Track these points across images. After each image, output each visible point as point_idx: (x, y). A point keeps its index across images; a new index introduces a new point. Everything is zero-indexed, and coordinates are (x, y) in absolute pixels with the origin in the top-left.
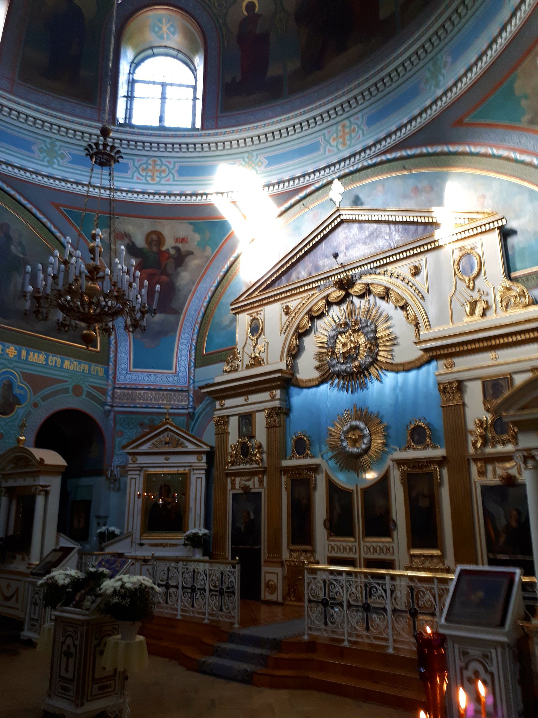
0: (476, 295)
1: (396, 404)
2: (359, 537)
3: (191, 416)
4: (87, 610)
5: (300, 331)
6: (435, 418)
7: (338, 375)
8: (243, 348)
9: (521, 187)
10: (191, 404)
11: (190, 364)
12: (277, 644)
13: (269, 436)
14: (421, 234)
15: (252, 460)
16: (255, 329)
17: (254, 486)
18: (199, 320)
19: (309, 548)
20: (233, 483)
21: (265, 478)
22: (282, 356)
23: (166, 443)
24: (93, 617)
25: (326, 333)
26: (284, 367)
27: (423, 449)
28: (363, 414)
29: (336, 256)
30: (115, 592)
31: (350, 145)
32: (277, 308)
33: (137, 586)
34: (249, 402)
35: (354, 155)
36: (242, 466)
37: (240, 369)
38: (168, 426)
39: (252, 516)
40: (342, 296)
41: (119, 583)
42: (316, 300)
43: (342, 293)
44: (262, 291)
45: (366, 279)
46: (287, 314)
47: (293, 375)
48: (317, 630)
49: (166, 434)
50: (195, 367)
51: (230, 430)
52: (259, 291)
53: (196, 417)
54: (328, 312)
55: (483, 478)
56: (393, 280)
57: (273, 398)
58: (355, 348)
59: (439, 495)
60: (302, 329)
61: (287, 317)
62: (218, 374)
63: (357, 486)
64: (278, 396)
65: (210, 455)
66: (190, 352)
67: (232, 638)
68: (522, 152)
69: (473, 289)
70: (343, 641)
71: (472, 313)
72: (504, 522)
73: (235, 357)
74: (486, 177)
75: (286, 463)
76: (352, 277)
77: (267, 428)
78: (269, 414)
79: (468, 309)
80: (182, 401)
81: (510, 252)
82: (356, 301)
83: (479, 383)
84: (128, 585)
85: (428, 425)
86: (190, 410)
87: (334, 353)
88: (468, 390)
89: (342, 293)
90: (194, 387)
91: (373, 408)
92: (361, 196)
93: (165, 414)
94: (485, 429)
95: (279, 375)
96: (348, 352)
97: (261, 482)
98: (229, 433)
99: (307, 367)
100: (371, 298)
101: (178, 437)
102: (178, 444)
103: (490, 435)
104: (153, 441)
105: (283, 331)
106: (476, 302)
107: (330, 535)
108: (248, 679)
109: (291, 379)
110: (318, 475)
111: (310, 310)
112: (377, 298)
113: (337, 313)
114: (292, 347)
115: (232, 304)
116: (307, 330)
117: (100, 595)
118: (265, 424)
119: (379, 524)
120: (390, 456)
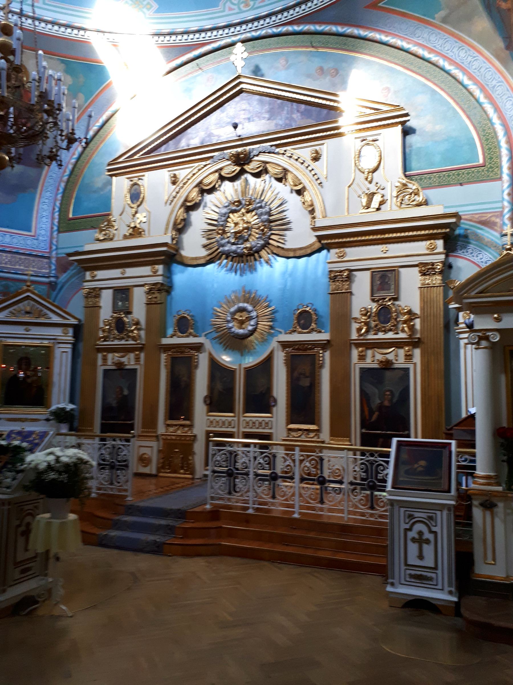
0: (373, 188)
1: (284, 290)
2: (239, 412)
3: (52, 286)
4: (8, 488)
5: (188, 204)
6: (321, 304)
7: (228, 255)
8: (121, 215)
9: (425, 85)
10: (53, 272)
11: (52, 228)
12: (181, 514)
13: (148, 313)
14: (317, 120)
15: (129, 337)
16: (136, 196)
17: (129, 362)
18: (65, 178)
19: (187, 422)
20: (105, 359)
21: (142, 355)
22: (167, 229)
23: (28, 313)
24: (17, 495)
25: (217, 210)
26: (169, 241)
27: (309, 333)
28: (251, 297)
29: (235, 126)
30: (50, 468)
31: (254, 5)
32: (165, 174)
33: (74, 460)
34: (126, 275)
35: (257, 19)
36: (116, 342)
37: (115, 239)
38: (29, 294)
39: (126, 392)
40: (236, 172)
41: (51, 458)
42: (207, 173)
43: (238, 168)
44: (142, 155)
45: (263, 158)
46: (174, 183)
47: (177, 250)
48: (220, 499)
49: (26, 302)
50: (59, 232)
51: (102, 304)
52: (141, 153)
53: (59, 287)
54: (220, 186)
55: (358, 362)
56: (292, 161)
57: (155, 273)
58: (247, 228)
59: (320, 375)
60: (190, 202)
61: (175, 186)
62: (88, 242)
63: (240, 365)
64: (160, 272)
65: (78, 329)
66: (53, 213)
67: (131, 510)
68: (431, 51)
69: (370, 182)
70: (247, 508)
71: (368, 207)
72: (378, 401)
73: (110, 225)
74: (391, 69)
75: (165, 341)
76: (250, 153)
77: (147, 304)
78: (150, 290)
79: (364, 201)
80: (41, 268)
81: (407, 150)
82: (251, 179)
83: (368, 274)
84: (64, 459)
85: (315, 310)
86: (52, 279)
87: (224, 232)
88: (356, 279)
89: (238, 168)
90: (57, 254)
91: (262, 292)
92: (262, 66)
93: (25, 281)
94: (369, 317)
95: (165, 249)
96: (240, 232)
97: (137, 359)
98: (100, 307)
99: (193, 245)
100: (267, 177)
101: (41, 307)
102: (41, 315)
103: (373, 324)
104: (11, 309)
105: (169, 202)
106: (373, 194)
107: (210, 410)
108: (157, 549)
109: (175, 255)
110: (201, 353)
111: (201, 182)
112: (273, 179)
113: (229, 190)
114: (179, 221)
115: (109, 165)
116: (196, 203)
117: (22, 471)
118: (144, 300)
119: (260, 400)
120: (276, 339)
